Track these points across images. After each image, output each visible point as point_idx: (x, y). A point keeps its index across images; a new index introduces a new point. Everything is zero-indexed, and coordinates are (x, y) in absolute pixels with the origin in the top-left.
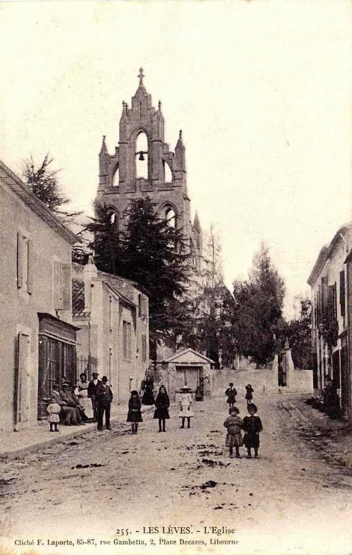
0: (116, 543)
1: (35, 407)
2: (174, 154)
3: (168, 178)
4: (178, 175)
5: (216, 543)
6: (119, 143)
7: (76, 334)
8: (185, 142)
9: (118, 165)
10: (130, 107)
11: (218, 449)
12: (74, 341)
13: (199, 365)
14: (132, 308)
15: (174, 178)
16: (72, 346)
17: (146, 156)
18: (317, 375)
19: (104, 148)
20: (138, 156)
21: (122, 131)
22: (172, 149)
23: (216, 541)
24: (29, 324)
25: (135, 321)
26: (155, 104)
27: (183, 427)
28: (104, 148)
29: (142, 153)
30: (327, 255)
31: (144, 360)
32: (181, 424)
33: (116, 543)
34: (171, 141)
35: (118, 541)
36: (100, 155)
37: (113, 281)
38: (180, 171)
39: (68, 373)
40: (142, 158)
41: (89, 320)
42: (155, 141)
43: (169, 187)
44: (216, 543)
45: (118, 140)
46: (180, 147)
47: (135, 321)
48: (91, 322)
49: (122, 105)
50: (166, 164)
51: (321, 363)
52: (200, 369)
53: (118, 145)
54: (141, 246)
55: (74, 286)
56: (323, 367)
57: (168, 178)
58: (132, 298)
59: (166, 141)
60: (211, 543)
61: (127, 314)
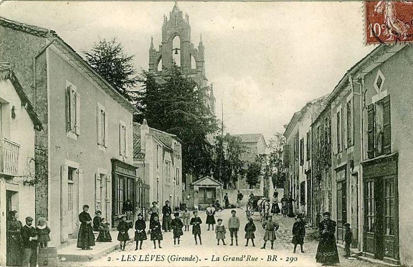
0: (225, 259)
1: (32, 205)
3: (194, 66)
4: (199, 64)
6: (162, 43)
7: (136, 171)
9: (161, 57)
10: (168, 19)
12: (134, 175)
13: (213, 187)
14: (171, 151)
15: (197, 67)
16: (133, 179)
17: (179, 51)
18: (330, 151)
20: (174, 52)
22: (196, 46)
25: (172, 159)
26: (184, 18)
27: (232, 245)
29: (177, 49)
30: (297, 118)
31: (178, 184)
32: (231, 243)
33: (225, 259)
35: (228, 258)
37: (158, 132)
38: (200, 62)
40: (176, 53)
41: (144, 161)
42: (185, 42)
43: (196, 72)
46: (201, 46)
47: (172, 159)
48: (145, 162)
50: (192, 56)
51: (292, 187)
52: (214, 189)
54: (171, 104)
55: (134, 137)
57: (194, 66)
58: (171, 145)
61: (168, 155)
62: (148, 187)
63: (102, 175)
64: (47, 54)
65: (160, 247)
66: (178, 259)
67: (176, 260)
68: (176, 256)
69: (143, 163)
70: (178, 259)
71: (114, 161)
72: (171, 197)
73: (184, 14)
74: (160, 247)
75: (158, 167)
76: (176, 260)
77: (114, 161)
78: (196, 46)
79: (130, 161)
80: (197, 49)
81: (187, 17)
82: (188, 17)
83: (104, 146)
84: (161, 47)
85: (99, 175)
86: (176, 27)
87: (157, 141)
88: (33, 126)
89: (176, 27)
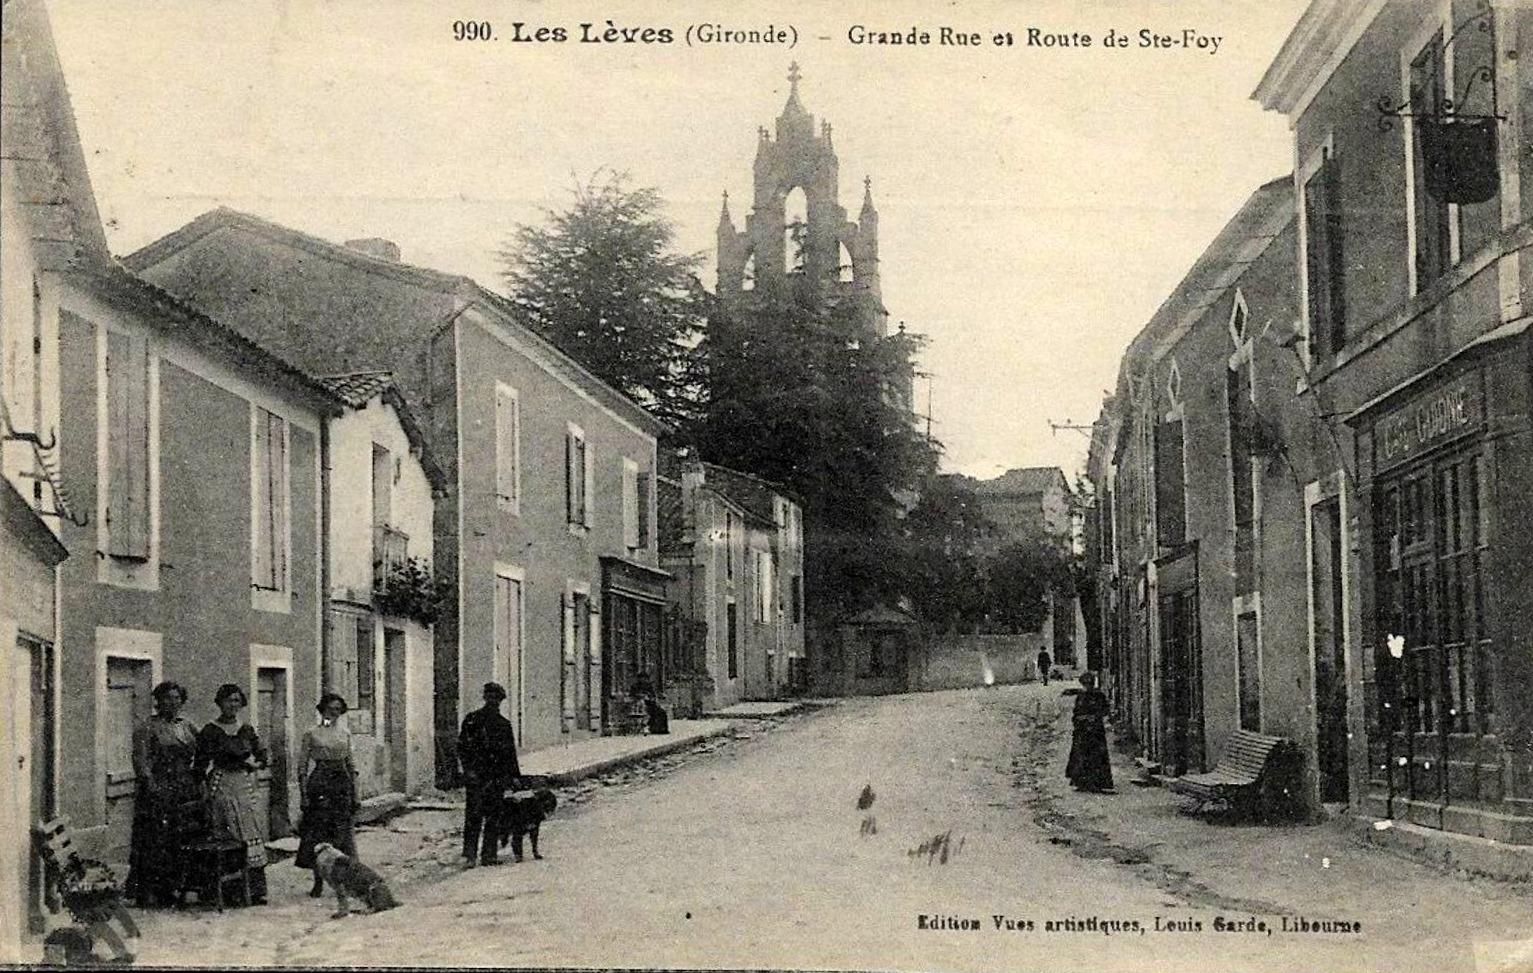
2: (856, 226)
5: (1300, 927)
6: (754, 208)
8: (876, 202)
10: (773, 139)
11: (670, 587)
19: (726, 217)
20: (789, 232)
21: (760, 185)
22: (853, 216)
23: (1299, 921)
24: (584, 576)
26: (818, 133)
28: (726, 217)
34: (389, 406)
36: (719, 231)
38: (866, 261)
39: (120, 431)
44: (1300, 927)
45: (752, 202)
46: (868, 211)
49: (758, 134)
53: (752, 212)
56: (574, 490)
59: (842, 202)
60: (1285, 929)
62: (702, 627)
63: (577, 597)
64: (457, 332)
65: (538, 857)
66: (723, 37)
67: (715, 38)
68: (715, 26)
69: (688, 563)
70: (723, 37)
71: (607, 563)
72: (770, 656)
73: (817, 122)
74: (538, 857)
75: (730, 573)
76: (715, 38)
77: (607, 563)
78: (853, 216)
79: (647, 558)
80: (858, 223)
81: (827, 128)
82: (830, 129)
83: (582, 524)
84: (750, 219)
85: (571, 597)
86: (796, 155)
87: (727, 503)
88: (430, 493)
89: (796, 155)
